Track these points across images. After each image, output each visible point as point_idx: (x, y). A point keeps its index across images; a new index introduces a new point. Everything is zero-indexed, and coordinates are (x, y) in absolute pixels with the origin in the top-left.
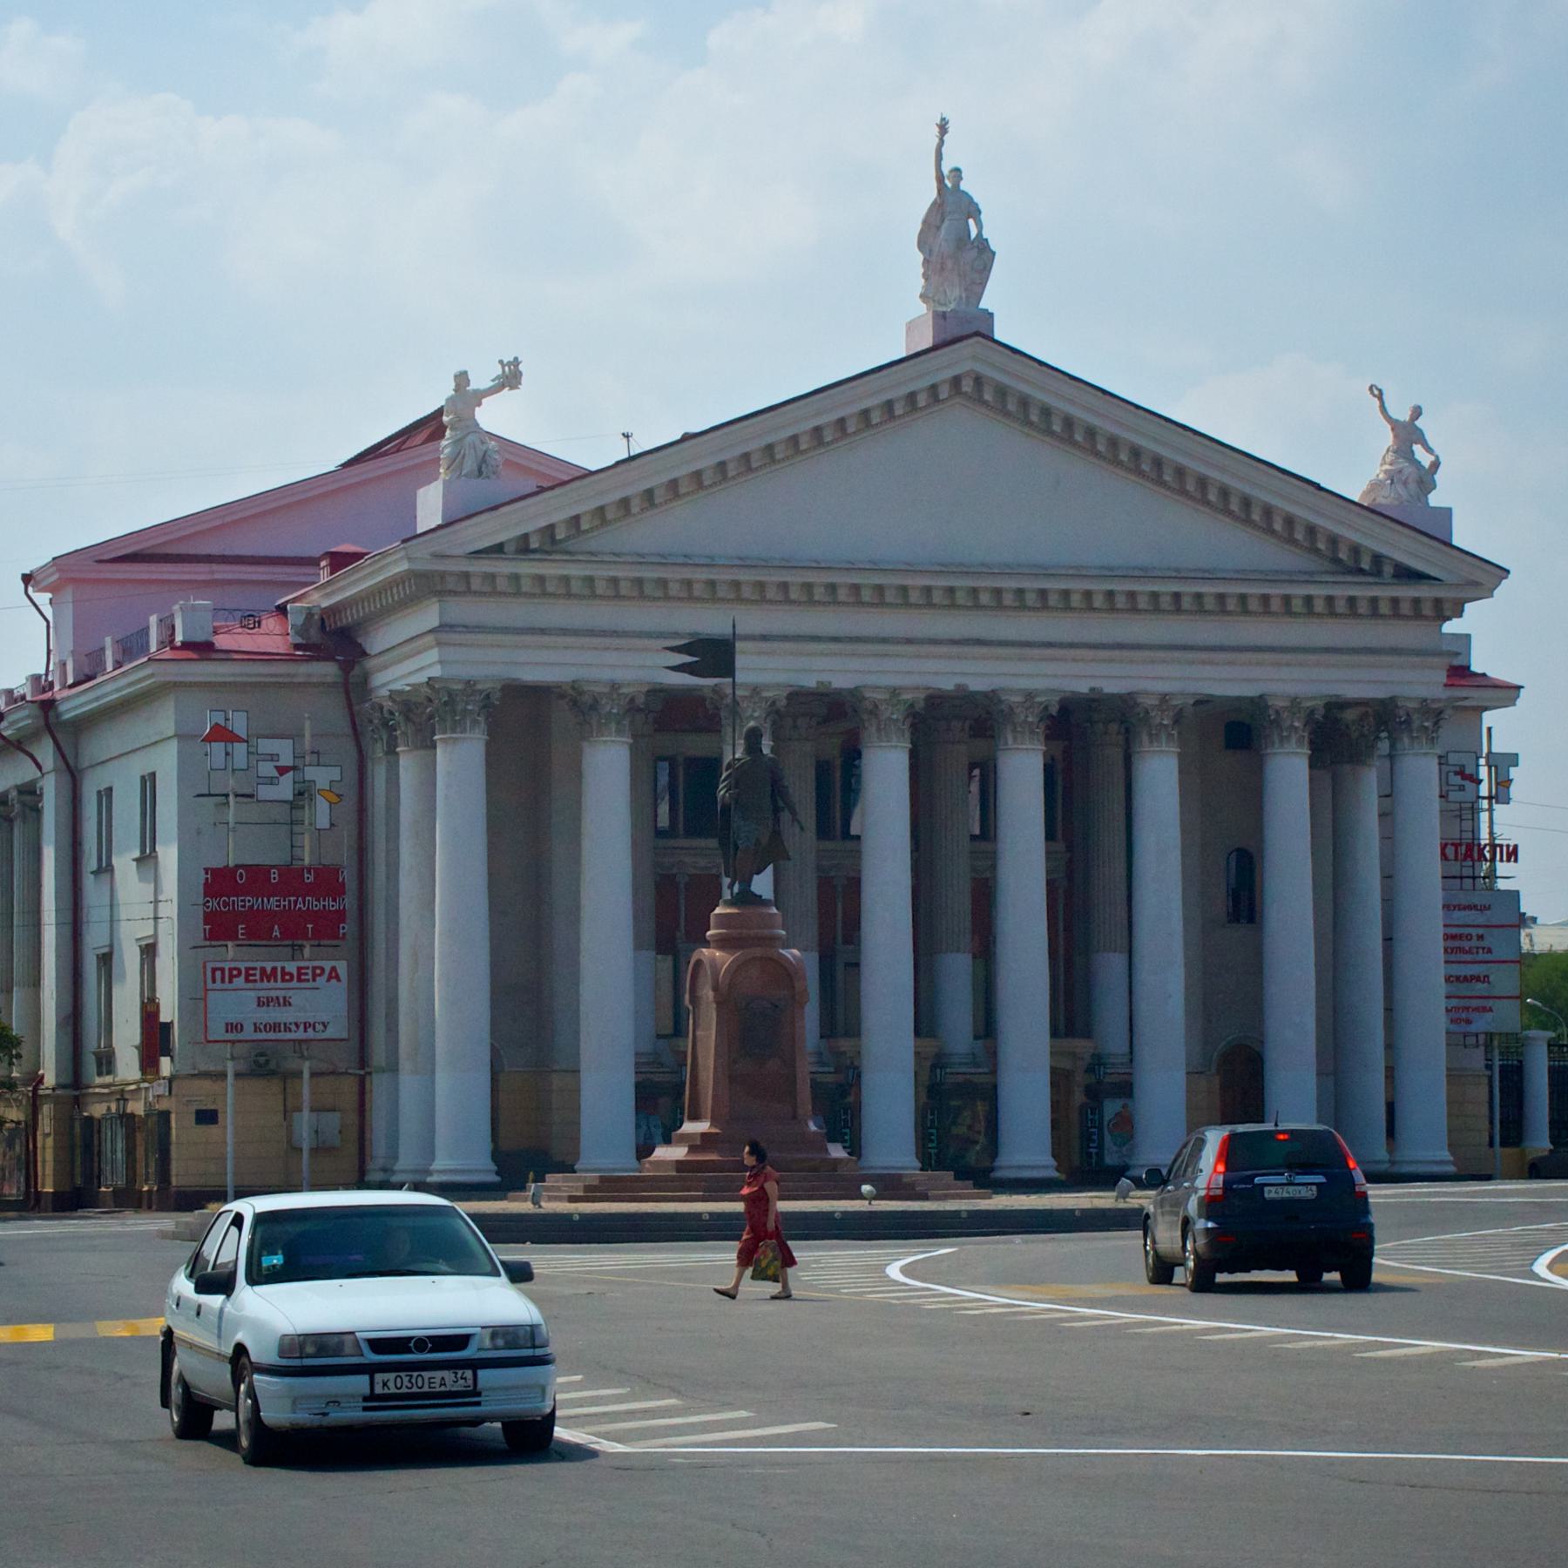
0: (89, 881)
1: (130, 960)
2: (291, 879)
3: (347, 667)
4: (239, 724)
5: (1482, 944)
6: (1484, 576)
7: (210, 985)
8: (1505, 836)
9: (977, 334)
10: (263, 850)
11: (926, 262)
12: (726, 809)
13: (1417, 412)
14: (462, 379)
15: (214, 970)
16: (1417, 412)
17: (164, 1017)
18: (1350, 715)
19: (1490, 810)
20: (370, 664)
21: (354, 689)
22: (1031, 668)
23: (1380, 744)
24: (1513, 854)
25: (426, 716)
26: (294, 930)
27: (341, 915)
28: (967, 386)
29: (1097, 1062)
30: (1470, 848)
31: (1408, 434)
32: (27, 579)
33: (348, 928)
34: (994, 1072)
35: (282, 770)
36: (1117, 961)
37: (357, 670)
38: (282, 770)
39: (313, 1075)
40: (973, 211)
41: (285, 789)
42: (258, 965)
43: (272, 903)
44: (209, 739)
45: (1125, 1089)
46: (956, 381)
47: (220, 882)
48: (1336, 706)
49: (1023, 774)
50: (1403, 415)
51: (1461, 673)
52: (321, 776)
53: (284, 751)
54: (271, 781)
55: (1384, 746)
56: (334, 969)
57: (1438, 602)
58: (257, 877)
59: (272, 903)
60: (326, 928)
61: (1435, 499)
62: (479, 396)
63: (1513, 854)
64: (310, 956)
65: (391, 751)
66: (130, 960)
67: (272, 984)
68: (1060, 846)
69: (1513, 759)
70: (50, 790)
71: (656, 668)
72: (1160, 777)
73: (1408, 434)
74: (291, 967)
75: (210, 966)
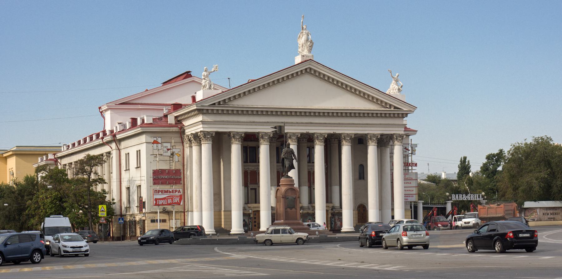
0: (123, 172)
1: (134, 189)
2: (169, 172)
4: (159, 140)
8: (415, 161)
10: (165, 167)
12: (283, 159)
17: (144, 201)
24: (416, 165)
28: (308, 70)
29: (333, 208)
33: (182, 182)
35: (168, 150)
38: (168, 150)
41: (169, 153)
44: (153, 143)
46: (306, 69)
47: (155, 172)
48: (382, 135)
49: (236, 150)
51: (406, 129)
52: (176, 151)
53: (169, 146)
57: (402, 114)
58: (162, 171)
63: (416, 165)
65: (191, 147)
69: (416, 145)
72: (346, 150)
74: (171, 190)
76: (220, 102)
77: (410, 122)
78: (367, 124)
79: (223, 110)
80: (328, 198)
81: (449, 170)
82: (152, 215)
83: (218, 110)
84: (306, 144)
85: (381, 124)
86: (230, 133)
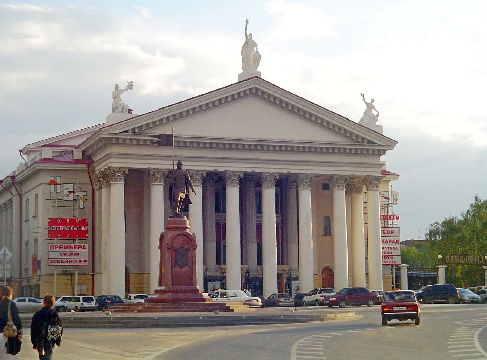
0: (23, 223)
1: (32, 244)
2: (73, 222)
3: (89, 166)
4: (58, 180)
5: (392, 260)
6: (391, 143)
7: (50, 250)
8: (396, 213)
9: (256, 77)
10: (67, 214)
11: (243, 58)
13: (373, 101)
14: (117, 87)
15: (51, 246)
16: (373, 101)
18: (356, 181)
19: (392, 206)
20: (95, 164)
21: (90, 171)
22: (271, 167)
23: (363, 189)
24: (398, 218)
25: (108, 177)
26: (73, 235)
27: (86, 232)
28: (254, 91)
30: (387, 216)
31: (370, 106)
32: (21, 151)
33: (89, 235)
34: (262, 274)
35: (70, 192)
36: (295, 245)
37: (92, 166)
38: (70, 192)
39: (78, 274)
40: (255, 44)
41: (71, 197)
42: (64, 245)
43: (67, 228)
44: (49, 184)
45: (297, 279)
47: (53, 222)
48: (352, 178)
49: (269, 195)
50: (369, 101)
52: (81, 194)
54: (68, 195)
55: (365, 188)
56: (84, 246)
57: (379, 150)
58: (63, 221)
59: (67, 228)
60: (83, 234)
61: (377, 123)
62: (122, 91)
64: (78, 242)
66: (32, 244)
67: (67, 250)
68: (280, 215)
70: (16, 200)
71: (169, 165)
73: (370, 106)
74: (72, 245)
75: (50, 245)
76: (134, 129)
77: (389, 160)
78: (332, 162)
79: (138, 140)
80: (282, 259)
81: (421, 236)
82: (48, 277)
83: (131, 140)
84: (254, 189)
85: (350, 163)
86: (148, 169)
